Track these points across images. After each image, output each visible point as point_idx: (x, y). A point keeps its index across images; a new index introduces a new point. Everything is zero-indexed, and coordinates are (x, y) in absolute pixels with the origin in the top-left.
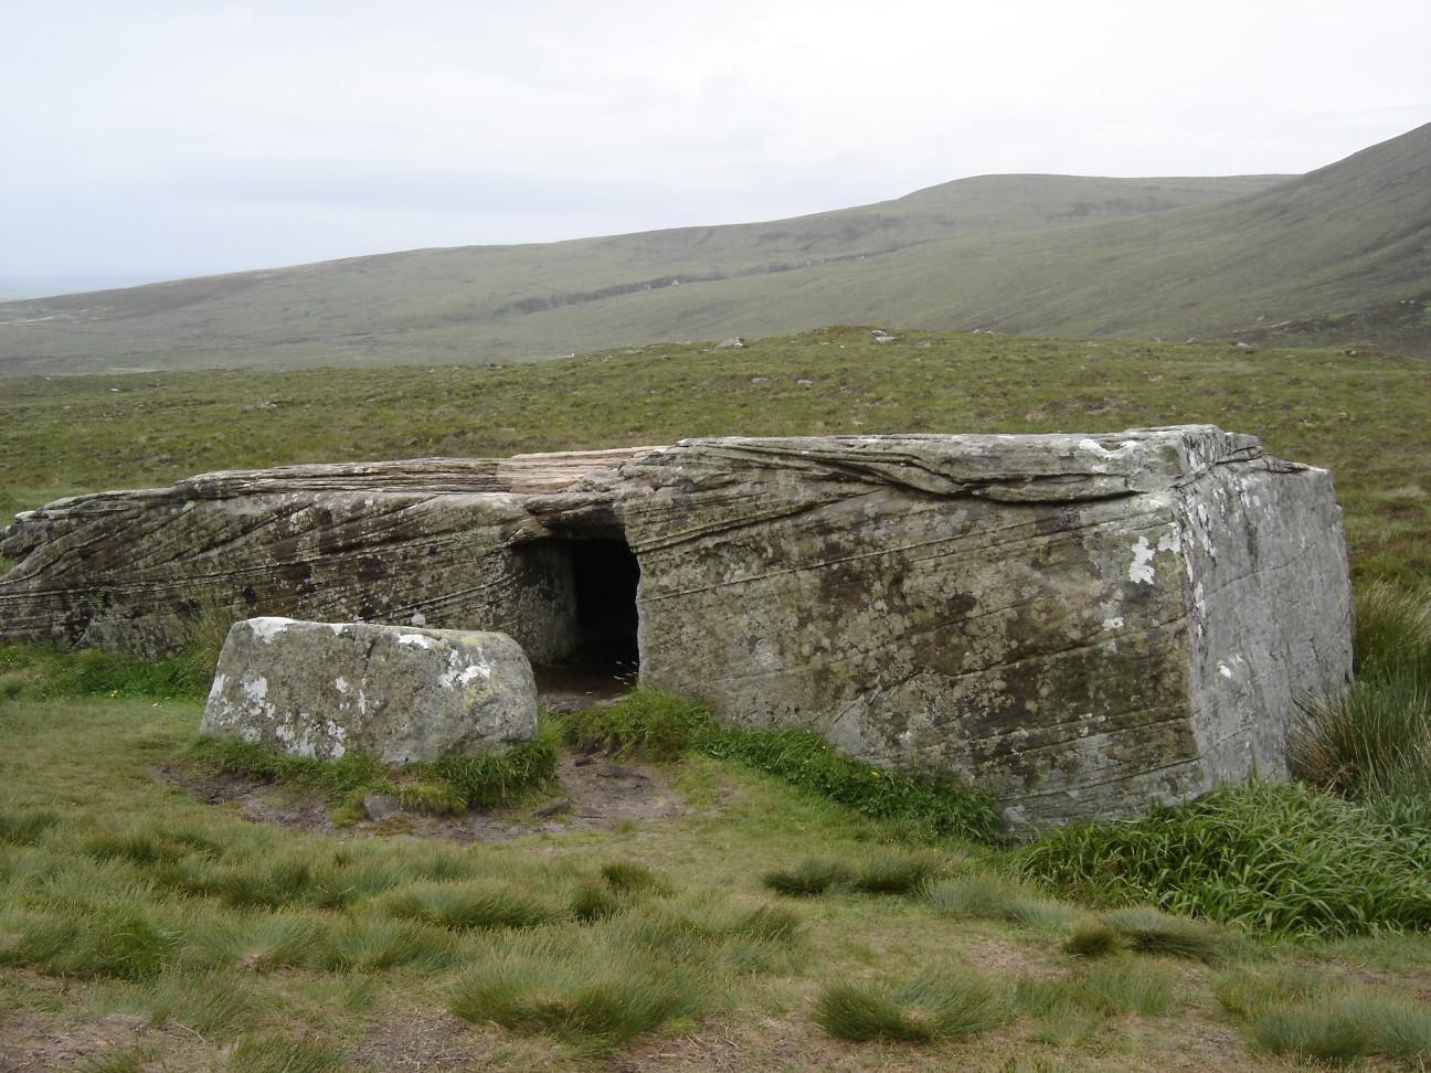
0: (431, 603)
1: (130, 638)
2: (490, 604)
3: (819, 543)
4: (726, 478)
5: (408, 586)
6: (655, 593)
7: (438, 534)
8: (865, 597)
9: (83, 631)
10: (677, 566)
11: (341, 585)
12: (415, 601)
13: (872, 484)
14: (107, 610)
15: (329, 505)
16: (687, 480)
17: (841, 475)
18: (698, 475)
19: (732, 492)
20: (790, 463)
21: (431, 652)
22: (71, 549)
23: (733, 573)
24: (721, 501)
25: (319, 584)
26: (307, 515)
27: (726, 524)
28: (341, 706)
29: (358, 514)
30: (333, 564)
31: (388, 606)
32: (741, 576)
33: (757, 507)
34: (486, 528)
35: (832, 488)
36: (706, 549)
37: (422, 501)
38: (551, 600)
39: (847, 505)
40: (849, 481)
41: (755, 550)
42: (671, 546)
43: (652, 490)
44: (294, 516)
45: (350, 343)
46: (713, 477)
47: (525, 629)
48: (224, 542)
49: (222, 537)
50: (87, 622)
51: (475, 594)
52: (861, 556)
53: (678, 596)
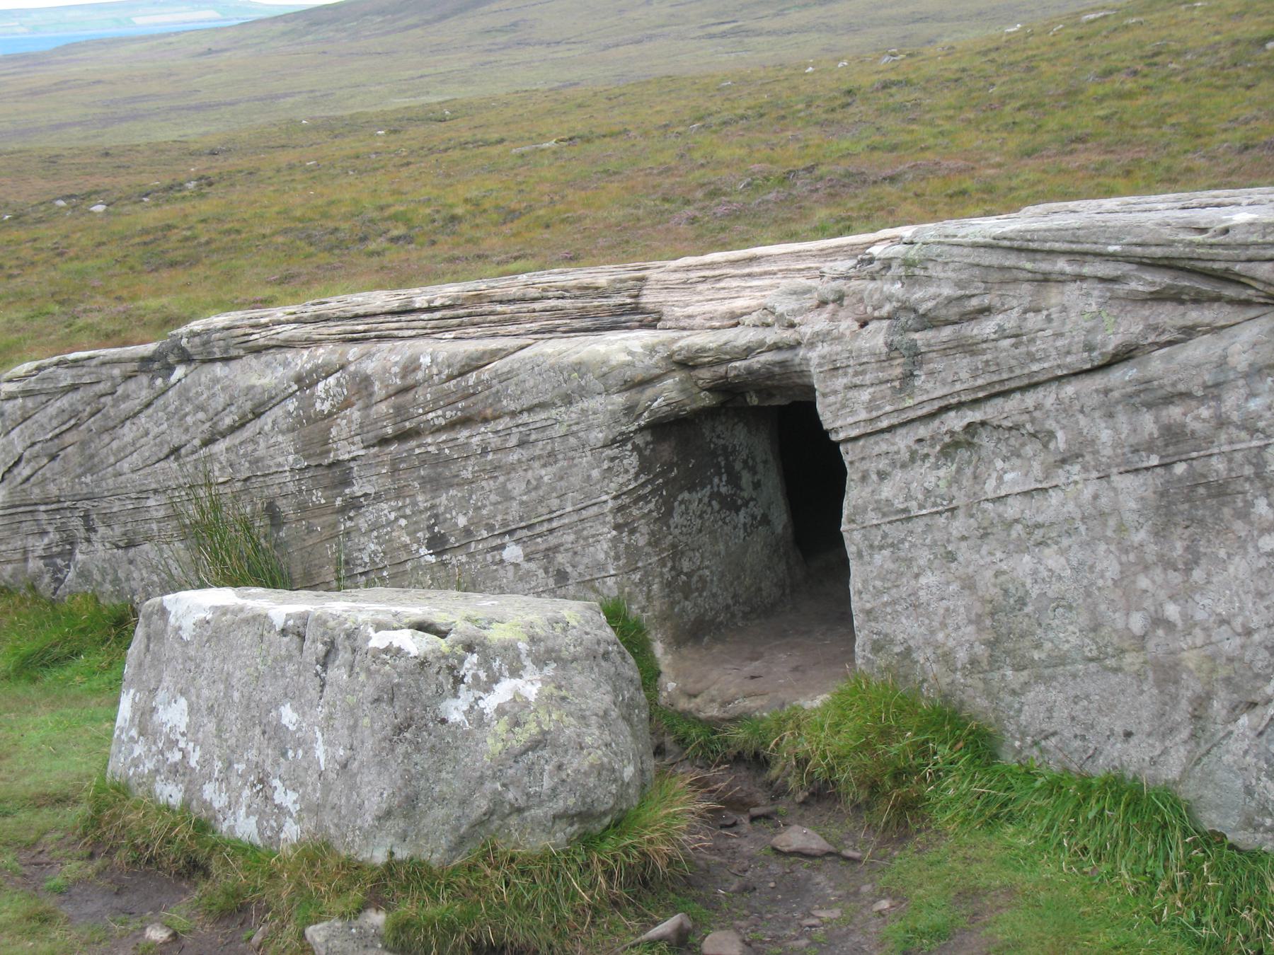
0: (529, 527)
1: (128, 580)
2: (617, 527)
3: (1148, 423)
4: (975, 302)
5: (493, 498)
6: (871, 514)
7: (530, 410)
8: (1240, 527)
9: (68, 566)
10: (903, 466)
11: (397, 498)
12: (505, 523)
13: (1247, 303)
14: (92, 535)
15: (370, 367)
16: (907, 308)
17: (1182, 290)
18: (924, 297)
19: (987, 327)
20: (1086, 270)
21: (423, 663)
22: (33, 444)
23: (1000, 478)
24: (968, 348)
25: (365, 495)
26: (339, 384)
27: (981, 388)
28: (291, 754)
29: (410, 380)
30: (382, 464)
31: (467, 532)
32: (1014, 482)
33: (1032, 358)
34: (600, 399)
35: (1170, 316)
36: (952, 433)
37: (508, 353)
38: (737, 510)
39: (1196, 350)
40: (1198, 300)
41: (1034, 435)
42: (890, 429)
43: (856, 326)
44: (321, 386)
45: (711, 36)
46: (950, 301)
47: (686, 565)
48: (233, 429)
49: (228, 421)
50: (71, 553)
51: (595, 510)
52: (1226, 448)
53: (909, 519)
